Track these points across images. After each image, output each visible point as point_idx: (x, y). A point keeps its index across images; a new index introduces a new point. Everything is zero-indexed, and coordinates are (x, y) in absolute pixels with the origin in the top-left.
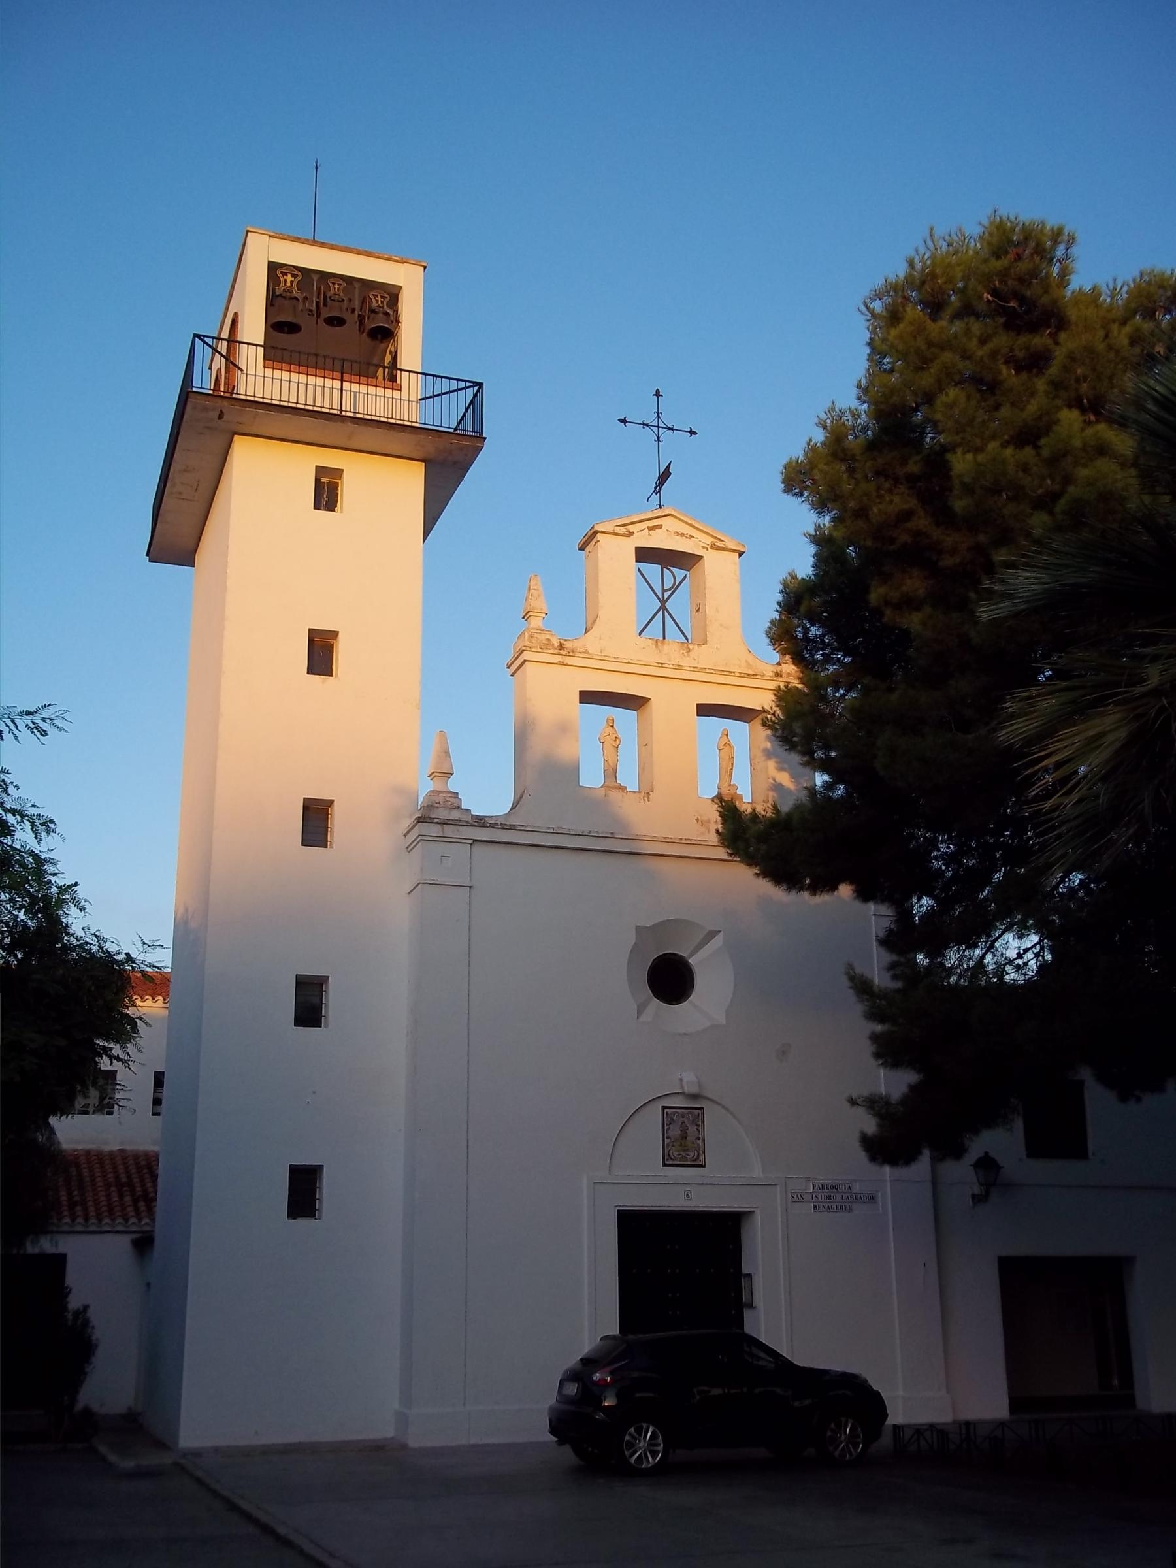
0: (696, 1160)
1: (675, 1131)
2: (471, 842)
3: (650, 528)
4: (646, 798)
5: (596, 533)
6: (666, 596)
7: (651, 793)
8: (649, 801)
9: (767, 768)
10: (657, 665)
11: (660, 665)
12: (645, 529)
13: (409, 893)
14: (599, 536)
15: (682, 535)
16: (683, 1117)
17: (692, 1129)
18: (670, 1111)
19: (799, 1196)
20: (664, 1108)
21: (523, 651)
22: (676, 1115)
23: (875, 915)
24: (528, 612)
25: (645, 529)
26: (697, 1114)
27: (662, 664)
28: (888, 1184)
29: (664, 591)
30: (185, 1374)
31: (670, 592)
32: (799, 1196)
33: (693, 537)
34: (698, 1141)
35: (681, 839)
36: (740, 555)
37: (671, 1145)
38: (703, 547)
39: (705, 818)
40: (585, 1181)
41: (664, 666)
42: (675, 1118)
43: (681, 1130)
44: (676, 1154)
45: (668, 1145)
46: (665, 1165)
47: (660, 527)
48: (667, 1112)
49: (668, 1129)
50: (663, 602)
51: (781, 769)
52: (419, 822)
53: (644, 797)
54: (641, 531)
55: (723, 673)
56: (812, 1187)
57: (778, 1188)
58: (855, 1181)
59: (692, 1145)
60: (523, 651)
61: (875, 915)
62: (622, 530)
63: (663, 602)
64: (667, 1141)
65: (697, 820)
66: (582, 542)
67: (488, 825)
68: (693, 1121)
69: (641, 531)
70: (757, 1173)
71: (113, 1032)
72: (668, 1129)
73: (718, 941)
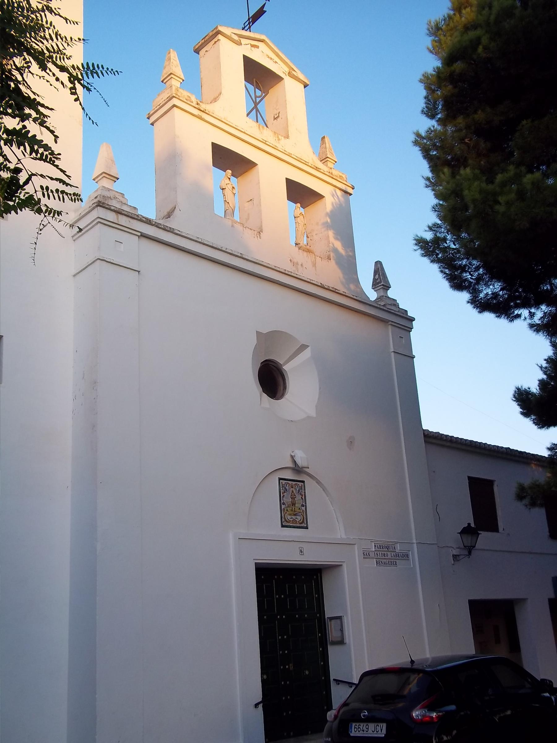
0: (301, 523)
1: (288, 499)
2: (139, 234)
3: (252, 46)
4: (258, 236)
5: (219, 32)
6: (258, 101)
7: (261, 233)
8: (260, 238)
9: (328, 237)
10: (262, 140)
11: (264, 141)
12: (248, 44)
13: (74, 276)
14: (220, 37)
15: (271, 59)
16: (292, 488)
17: (298, 497)
18: (284, 482)
19: (367, 554)
20: (280, 479)
21: (174, 97)
22: (288, 485)
23: (394, 352)
24: (171, 74)
25: (248, 44)
26: (300, 485)
27: (266, 141)
28: (415, 545)
29: (256, 97)
30: (534, 675)
31: (260, 98)
32: (367, 554)
33: (277, 63)
34: (302, 507)
35: (285, 270)
36: (305, 87)
37: (286, 509)
38: (284, 72)
39: (295, 261)
40: (231, 536)
41: (267, 143)
42: (287, 488)
43: (291, 498)
44: (289, 517)
45: (284, 509)
46: (283, 526)
47: (258, 47)
48: (282, 483)
49: (284, 496)
50: (256, 104)
51: (336, 239)
52: (97, 206)
53: (257, 234)
54: (246, 44)
55: (302, 161)
56: (374, 547)
57: (356, 547)
58: (397, 543)
59: (299, 510)
60: (174, 97)
61: (394, 352)
62: (236, 38)
63: (256, 104)
64: (283, 507)
65: (291, 261)
66: (199, 44)
67: (154, 223)
68: (299, 491)
69: (246, 44)
70: (340, 534)
71: (12, 23)
72: (284, 496)
73: (306, 354)
